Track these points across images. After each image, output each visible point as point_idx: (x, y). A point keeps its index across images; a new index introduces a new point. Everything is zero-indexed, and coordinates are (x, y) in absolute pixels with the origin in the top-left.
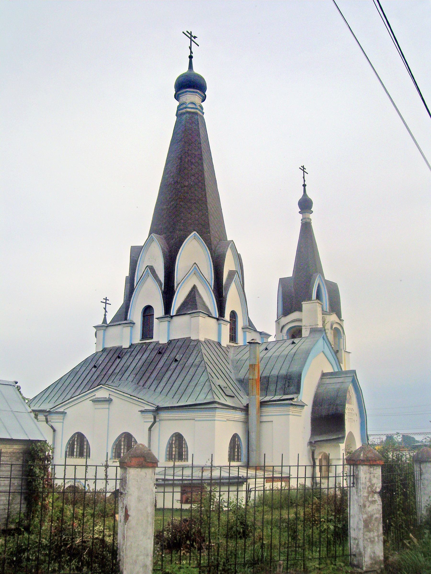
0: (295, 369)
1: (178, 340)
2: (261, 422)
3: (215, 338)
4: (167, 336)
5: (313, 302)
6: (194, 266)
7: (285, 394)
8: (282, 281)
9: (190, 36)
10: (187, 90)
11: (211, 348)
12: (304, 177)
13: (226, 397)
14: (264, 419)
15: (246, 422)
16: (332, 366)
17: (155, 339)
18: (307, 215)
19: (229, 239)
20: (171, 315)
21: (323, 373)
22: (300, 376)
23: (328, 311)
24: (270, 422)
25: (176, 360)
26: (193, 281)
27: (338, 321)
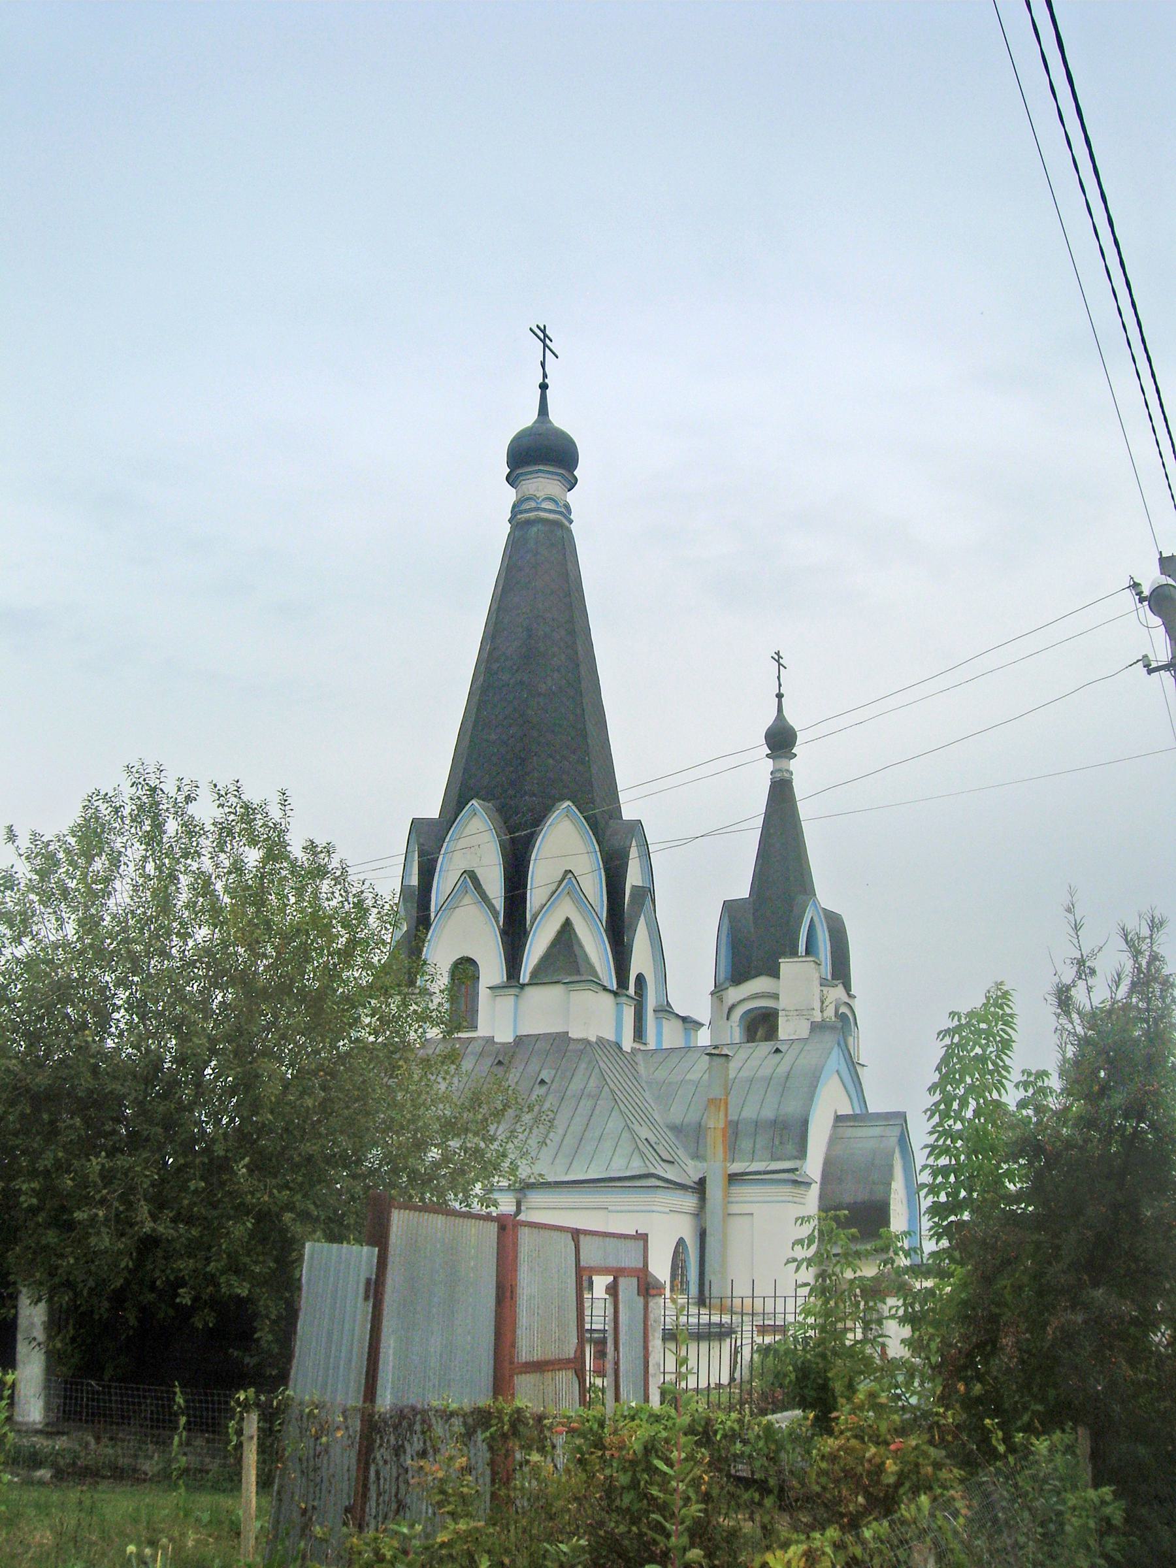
0: (791, 1107)
1: (538, 1037)
2: (729, 1214)
3: (610, 1035)
4: (512, 1027)
5: (800, 959)
6: (462, 879)
7: (774, 1158)
8: (730, 908)
9: (542, 336)
10: (541, 467)
11: (610, 1058)
12: (779, 678)
13: (661, 1163)
14: (734, 1209)
15: (700, 1213)
16: (849, 1096)
17: (483, 1031)
18: (783, 763)
19: (628, 814)
20: (521, 981)
21: (837, 1116)
22: (805, 1123)
23: (829, 977)
24: (746, 1217)
25: (542, 1082)
26: (566, 909)
27: (846, 999)
